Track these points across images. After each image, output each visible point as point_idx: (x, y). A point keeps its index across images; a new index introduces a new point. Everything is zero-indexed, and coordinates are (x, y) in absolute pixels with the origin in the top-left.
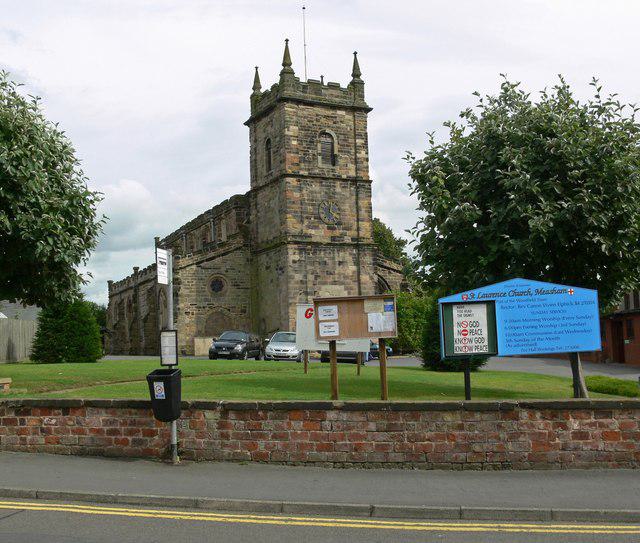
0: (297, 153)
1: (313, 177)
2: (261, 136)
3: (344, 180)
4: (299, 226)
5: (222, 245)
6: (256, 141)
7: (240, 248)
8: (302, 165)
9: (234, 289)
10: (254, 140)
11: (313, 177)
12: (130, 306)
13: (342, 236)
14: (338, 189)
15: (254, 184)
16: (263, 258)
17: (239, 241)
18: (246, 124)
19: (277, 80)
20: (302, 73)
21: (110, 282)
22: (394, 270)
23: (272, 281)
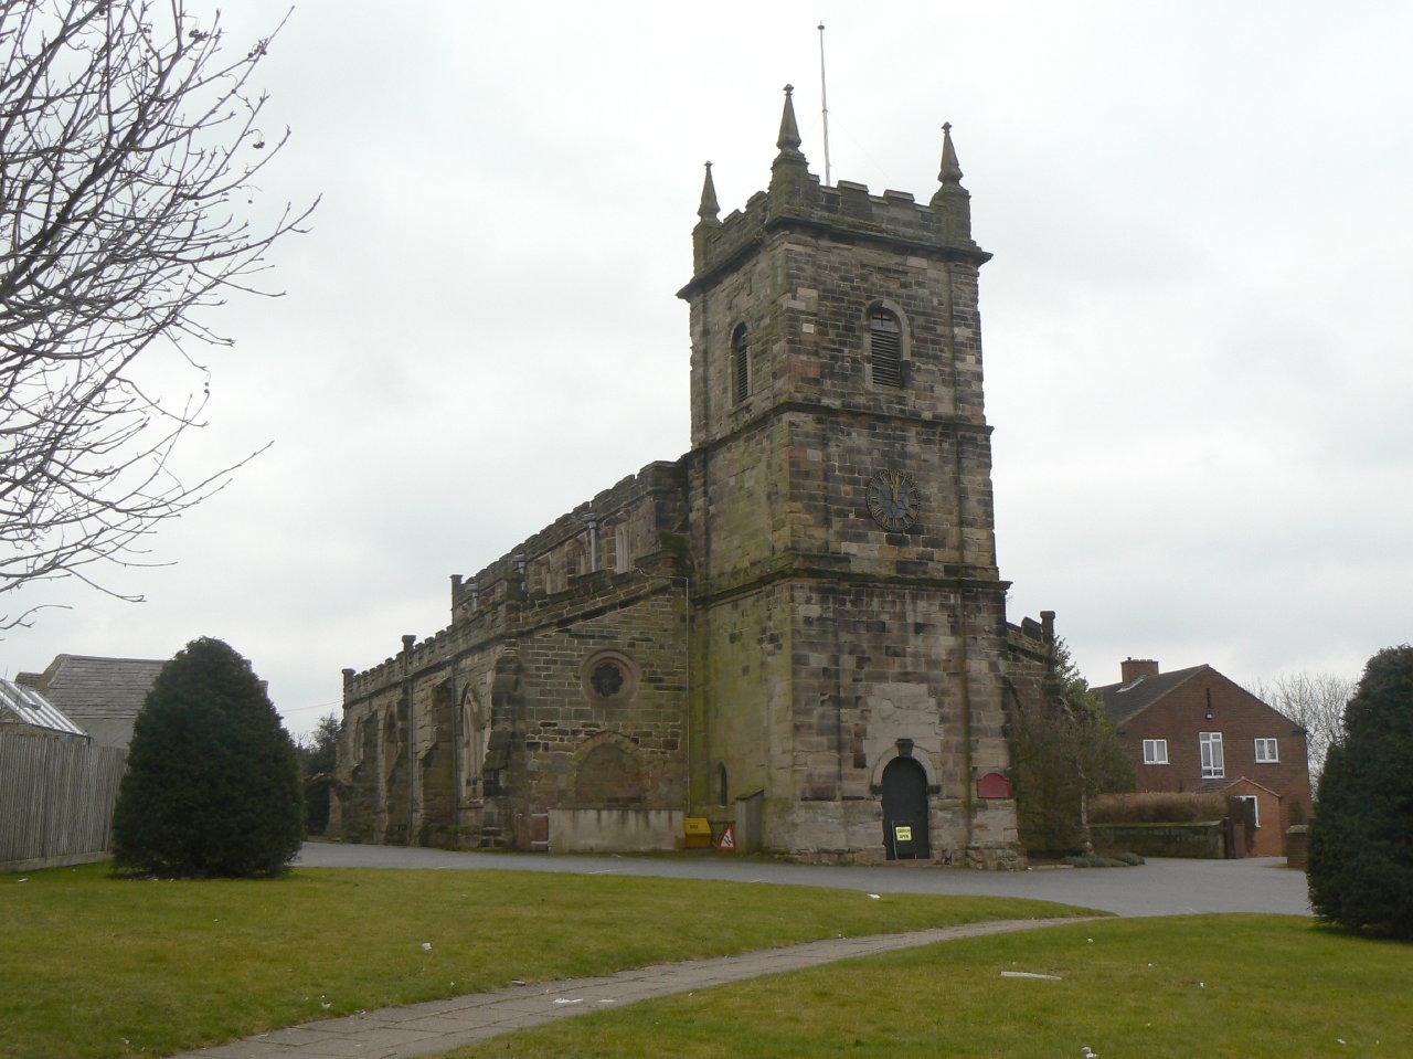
0: (816, 354)
1: (854, 413)
2: (721, 319)
3: (926, 424)
4: (819, 533)
5: (623, 580)
6: (705, 333)
7: (663, 590)
8: (827, 384)
9: (650, 689)
10: (702, 332)
11: (854, 413)
12: (390, 726)
13: (924, 560)
14: (913, 447)
15: (702, 436)
16: (723, 616)
17: (663, 575)
18: (683, 294)
19: (762, 181)
20: (831, 164)
21: (348, 673)
22: (1027, 653)
23: (746, 670)
